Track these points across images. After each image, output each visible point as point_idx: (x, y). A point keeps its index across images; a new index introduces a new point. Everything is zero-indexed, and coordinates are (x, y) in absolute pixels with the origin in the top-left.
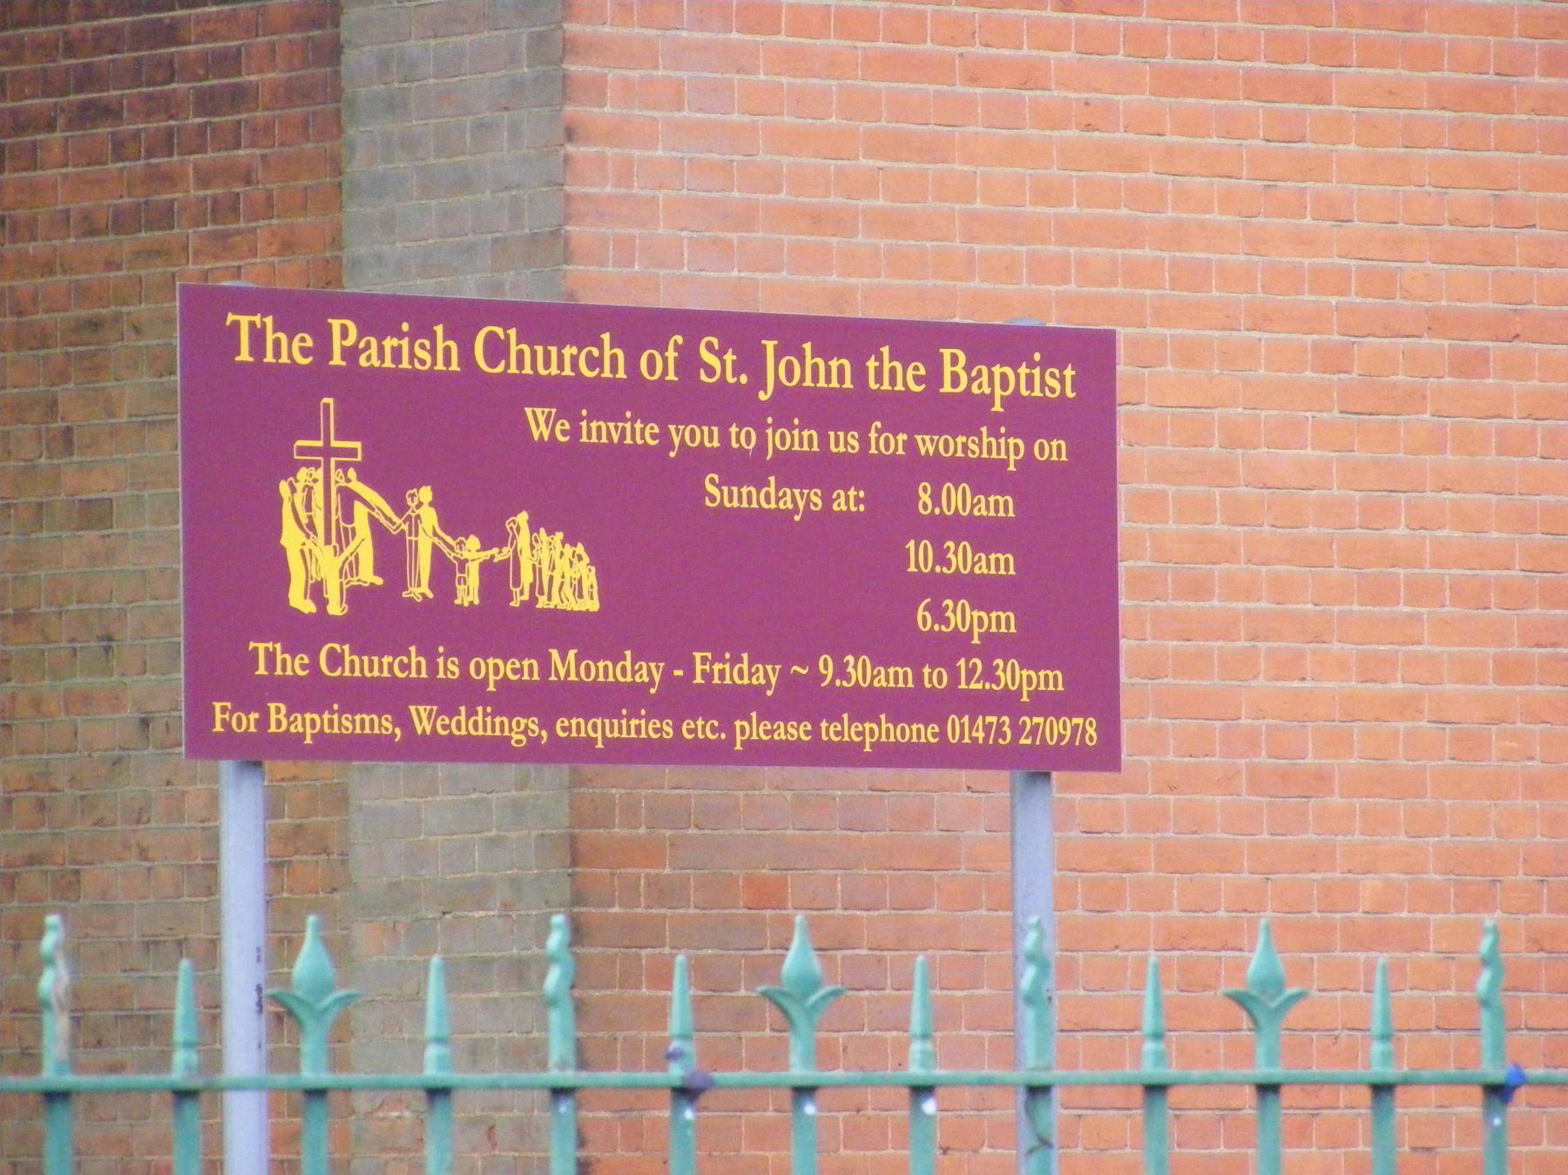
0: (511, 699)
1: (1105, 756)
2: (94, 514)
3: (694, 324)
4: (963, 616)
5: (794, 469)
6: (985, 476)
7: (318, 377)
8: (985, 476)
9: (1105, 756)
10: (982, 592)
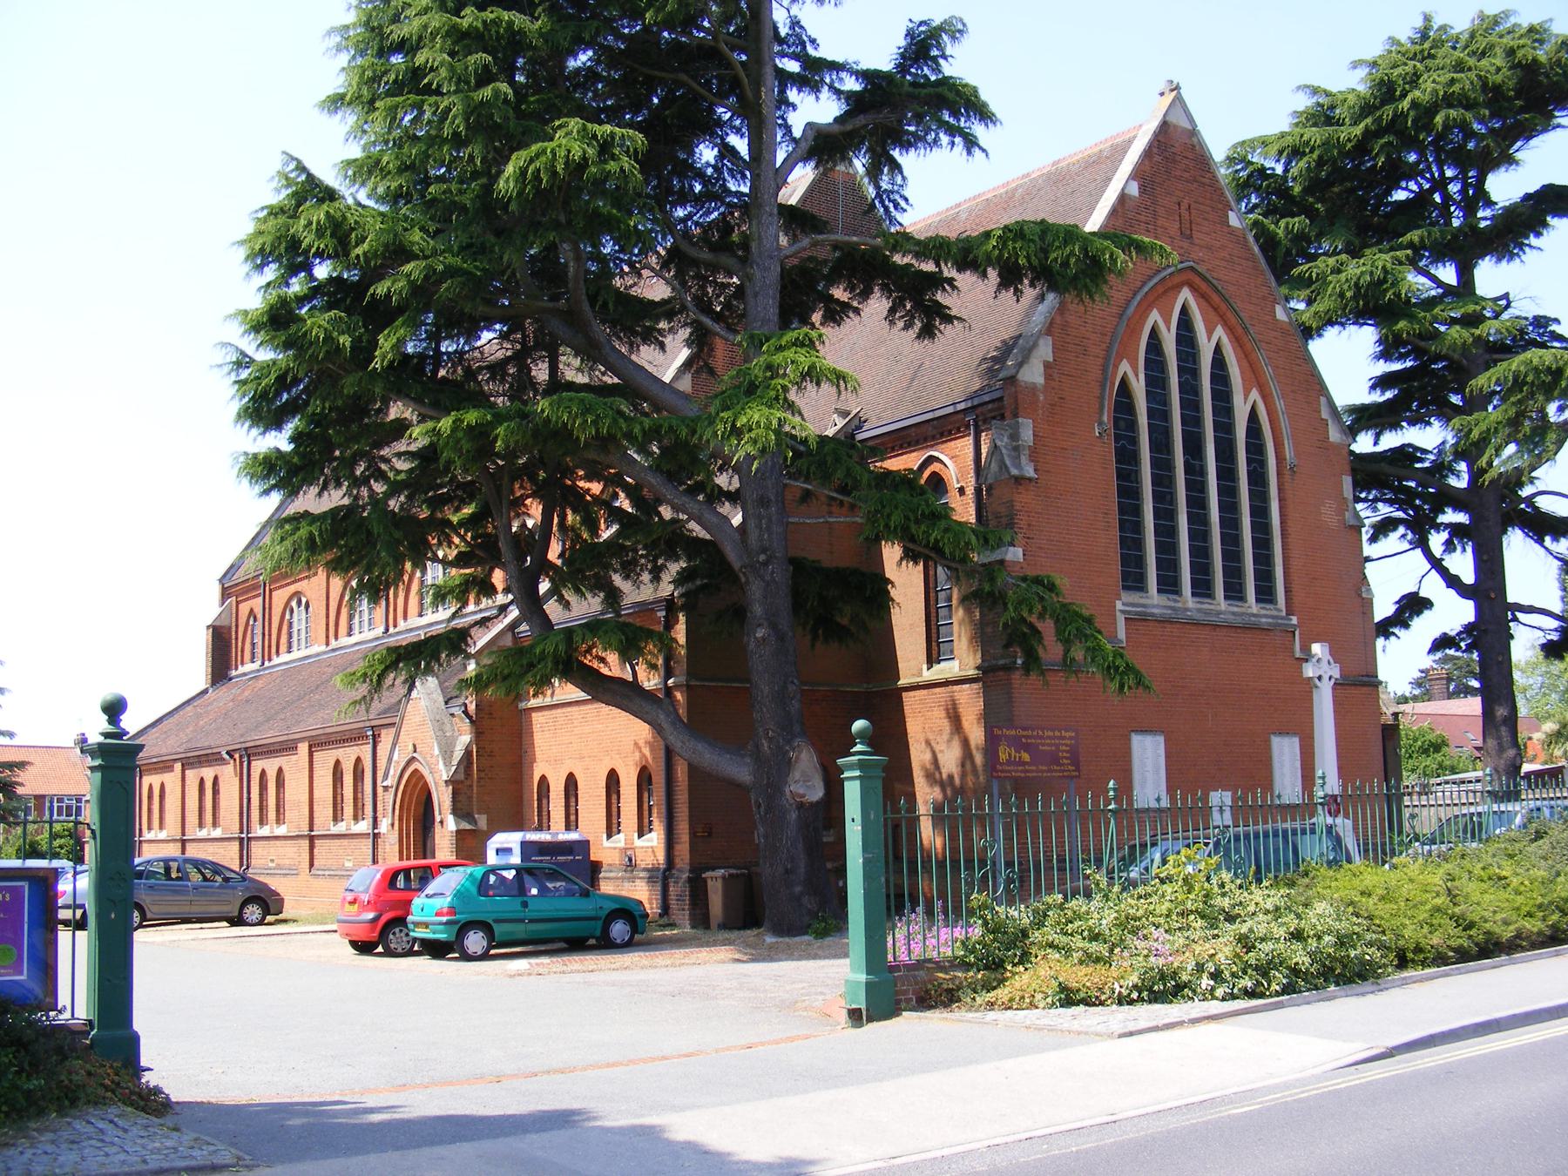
1: (1079, 777)
5: (1048, 745)
9: (1079, 777)
10: (1066, 758)
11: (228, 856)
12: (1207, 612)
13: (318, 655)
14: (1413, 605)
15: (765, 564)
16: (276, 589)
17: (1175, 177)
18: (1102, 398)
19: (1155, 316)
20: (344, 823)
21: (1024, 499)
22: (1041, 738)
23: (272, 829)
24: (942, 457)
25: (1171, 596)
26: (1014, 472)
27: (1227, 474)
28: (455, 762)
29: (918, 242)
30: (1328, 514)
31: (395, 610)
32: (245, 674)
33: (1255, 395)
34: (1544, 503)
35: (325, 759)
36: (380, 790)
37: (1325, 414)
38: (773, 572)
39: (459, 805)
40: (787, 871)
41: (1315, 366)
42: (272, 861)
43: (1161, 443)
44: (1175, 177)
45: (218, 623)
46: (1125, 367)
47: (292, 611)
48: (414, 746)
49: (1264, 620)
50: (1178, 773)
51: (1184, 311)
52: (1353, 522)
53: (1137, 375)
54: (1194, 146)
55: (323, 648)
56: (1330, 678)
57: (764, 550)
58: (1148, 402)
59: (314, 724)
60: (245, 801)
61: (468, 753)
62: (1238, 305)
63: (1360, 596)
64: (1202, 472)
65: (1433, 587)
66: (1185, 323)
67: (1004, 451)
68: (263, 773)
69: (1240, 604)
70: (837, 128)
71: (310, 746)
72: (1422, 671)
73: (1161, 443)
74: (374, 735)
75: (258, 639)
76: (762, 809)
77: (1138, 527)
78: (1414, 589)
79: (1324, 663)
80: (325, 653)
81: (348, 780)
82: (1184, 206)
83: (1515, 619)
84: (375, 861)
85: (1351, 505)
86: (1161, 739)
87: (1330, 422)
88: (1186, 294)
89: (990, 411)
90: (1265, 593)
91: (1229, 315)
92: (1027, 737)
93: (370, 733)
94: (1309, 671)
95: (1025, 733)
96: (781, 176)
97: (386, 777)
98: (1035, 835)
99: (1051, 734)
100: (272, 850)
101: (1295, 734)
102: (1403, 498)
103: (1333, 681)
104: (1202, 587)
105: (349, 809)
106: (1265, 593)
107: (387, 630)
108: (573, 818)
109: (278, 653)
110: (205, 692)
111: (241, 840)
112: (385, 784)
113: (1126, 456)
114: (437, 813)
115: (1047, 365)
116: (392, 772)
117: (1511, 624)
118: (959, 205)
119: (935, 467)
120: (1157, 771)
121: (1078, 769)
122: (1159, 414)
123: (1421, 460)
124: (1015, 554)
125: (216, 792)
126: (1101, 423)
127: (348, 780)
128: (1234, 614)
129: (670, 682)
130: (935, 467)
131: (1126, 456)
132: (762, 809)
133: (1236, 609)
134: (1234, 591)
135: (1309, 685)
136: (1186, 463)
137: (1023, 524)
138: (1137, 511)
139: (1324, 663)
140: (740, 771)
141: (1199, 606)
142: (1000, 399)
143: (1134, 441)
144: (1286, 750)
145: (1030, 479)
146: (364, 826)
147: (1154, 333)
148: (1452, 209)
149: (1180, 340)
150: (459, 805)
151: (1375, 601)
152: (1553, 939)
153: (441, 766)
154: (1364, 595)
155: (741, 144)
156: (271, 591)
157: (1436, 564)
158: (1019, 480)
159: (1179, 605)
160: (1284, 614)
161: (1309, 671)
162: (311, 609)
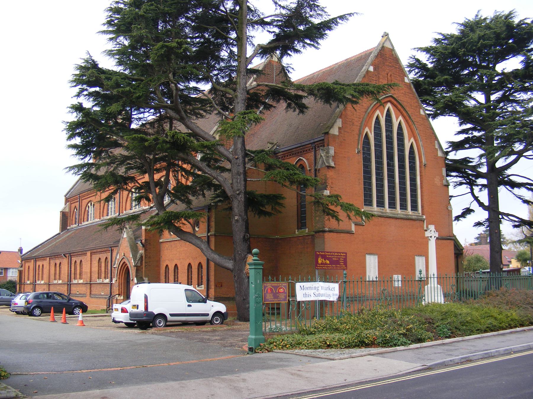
0: (326, 267)
1: (347, 269)
2: (301, 259)
3: (332, 252)
4: (342, 264)
5: (336, 258)
6: (342, 258)
7: (319, 254)
8: (342, 258)
9: (347, 269)
10: (342, 263)
11: (64, 290)
13: (97, 222)
14: (468, 211)
15: (239, 194)
16: (83, 199)
17: (386, 65)
18: (359, 140)
19: (378, 112)
21: (330, 174)
22: (333, 255)
23: (78, 281)
24: (304, 159)
26: (327, 164)
27: (402, 167)
28: (137, 260)
29: (295, 85)
31: (122, 208)
32: (72, 228)
33: (412, 140)
34: (512, 178)
35: (96, 257)
36: (113, 269)
37: (437, 147)
38: (241, 198)
39: (138, 274)
40: (244, 299)
42: (78, 292)
43: (379, 156)
44: (386, 65)
45: (63, 211)
46: (367, 130)
48: (124, 254)
49: (413, 217)
51: (388, 110)
52: (446, 184)
53: (371, 132)
54: (393, 55)
56: (435, 237)
57: (238, 190)
58: (375, 141)
59: (92, 245)
60: (69, 271)
61: (142, 257)
62: (407, 109)
63: (448, 209)
64: (393, 166)
65: (475, 206)
66: (388, 115)
67: (324, 157)
68: (76, 262)
69: (405, 211)
70: (268, 46)
71: (91, 253)
72: (479, 235)
73: (379, 156)
74: (112, 250)
75: (77, 217)
76: (236, 278)
77: (370, 184)
78: (468, 207)
79: (432, 232)
81: (103, 265)
82: (389, 75)
83: (503, 218)
85: (445, 178)
86: (376, 257)
87: (438, 149)
88: (389, 105)
89: (320, 144)
90: (414, 207)
91: (404, 112)
92: (328, 255)
93: (110, 249)
94: (427, 234)
96: (249, 60)
97: (114, 264)
98: (496, 281)
100: (78, 288)
101: (424, 256)
102: (465, 176)
103: (436, 238)
104: (392, 205)
105: (103, 275)
106: (414, 207)
107: (119, 214)
109: (84, 221)
113: (367, 160)
114: (131, 277)
115: (340, 128)
116: (117, 263)
117: (502, 220)
118: (314, 73)
119: (301, 163)
121: (346, 266)
122: (378, 146)
123: (471, 162)
124: (327, 193)
125: (42, 269)
126: (358, 149)
127: (103, 265)
128: (403, 214)
129: (209, 234)
130: (301, 163)
131: (367, 160)
132: (236, 278)
133: (404, 213)
134: (403, 207)
135: (427, 239)
137: (330, 182)
138: (370, 178)
139: (432, 232)
140: (230, 264)
142: (323, 140)
143: (370, 155)
144: (420, 261)
145: (333, 167)
146: (107, 281)
147: (377, 118)
148: (484, 77)
149: (386, 120)
151: (453, 211)
154: (449, 209)
155: (235, 49)
156: (82, 200)
157: (476, 198)
158: (329, 167)
159: (384, 211)
160: (421, 215)
161: (427, 234)
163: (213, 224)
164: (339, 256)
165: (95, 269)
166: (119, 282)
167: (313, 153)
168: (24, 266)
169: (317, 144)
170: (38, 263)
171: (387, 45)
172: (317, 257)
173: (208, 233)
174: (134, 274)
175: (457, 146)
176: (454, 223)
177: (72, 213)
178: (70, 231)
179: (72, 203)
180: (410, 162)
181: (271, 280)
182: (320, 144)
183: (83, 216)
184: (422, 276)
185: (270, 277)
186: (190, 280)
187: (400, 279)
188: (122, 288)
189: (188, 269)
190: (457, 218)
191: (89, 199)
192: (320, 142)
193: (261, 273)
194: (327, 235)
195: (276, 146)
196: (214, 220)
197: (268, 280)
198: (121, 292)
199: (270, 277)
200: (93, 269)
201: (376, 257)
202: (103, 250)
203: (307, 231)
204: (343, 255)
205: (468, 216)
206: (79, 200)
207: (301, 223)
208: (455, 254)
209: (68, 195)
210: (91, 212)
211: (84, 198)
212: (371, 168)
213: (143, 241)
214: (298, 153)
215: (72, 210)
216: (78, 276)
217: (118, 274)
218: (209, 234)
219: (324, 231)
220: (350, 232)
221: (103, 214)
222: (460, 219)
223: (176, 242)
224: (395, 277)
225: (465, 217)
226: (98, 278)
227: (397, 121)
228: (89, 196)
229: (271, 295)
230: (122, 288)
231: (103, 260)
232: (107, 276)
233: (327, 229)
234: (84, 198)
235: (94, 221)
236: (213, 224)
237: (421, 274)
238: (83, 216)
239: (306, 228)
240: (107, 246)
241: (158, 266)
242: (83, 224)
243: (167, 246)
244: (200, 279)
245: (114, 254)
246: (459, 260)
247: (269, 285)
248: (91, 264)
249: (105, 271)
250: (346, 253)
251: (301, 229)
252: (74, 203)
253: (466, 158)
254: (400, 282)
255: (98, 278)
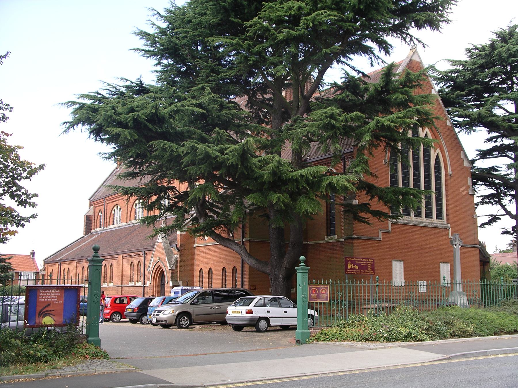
1: (374, 274)
4: (370, 269)
5: (364, 264)
6: (370, 264)
8: (370, 264)
9: (374, 274)
12: (419, 222)
13: (124, 226)
14: (494, 219)
16: (109, 203)
20: (107, 284)
23: (108, 284)
25: (407, 217)
27: (427, 177)
30: (463, 190)
32: (97, 232)
35: (127, 262)
36: (146, 272)
41: (460, 141)
47: (114, 211)
48: (159, 258)
49: (438, 225)
50: (408, 274)
55: (126, 224)
59: (123, 249)
61: (177, 261)
63: (473, 218)
64: (419, 176)
69: (431, 219)
74: (145, 254)
75: (102, 220)
76: (272, 282)
80: (126, 225)
81: (135, 268)
84: (144, 296)
86: (402, 263)
87: (464, 159)
90: (439, 216)
95: (357, 260)
97: (149, 268)
99: (365, 260)
105: (135, 278)
106: (439, 216)
108: (210, 282)
109: (109, 225)
110: (83, 237)
111: (144, 287)
112: (148, 270)
114: (166, 280)
116: (151, 266)
120: (401, 273)
121: (374, 272)
123: (499, 171)
126: (385, 160)
127: (135, 268)
128: (428, 223)
129: (244, 240)
132: (272, 282)
133: (429, 221)
134: (429, 215)
136: (414, 173)
141: (417, 220)
142: (353, 151)
144: (445, 268)
146: (140, 284)
150: (173, 278)
152: (515, 332)
153: (168, 265)
154: (474, 218)
156: (107, 204)
159: (410, 219)
160: (446, 223)
162: (121, 210)
163: (247, 230)
164: (368, 261)
165: (127, 272)
166: (153, 285)
167: (343, 163)
168: (46, 270)
169: (346, 156)
170: (63, 267)
171: (415, 58)
172: (347, 262)
173: (243, 239)
174: (170, 277)
175: (485, 154)
176: (479, 229)
177: (96, 216)
178: (94, 235)
179: (96, 207)
180: (435, 172)
181: (315, 283)
182: (349, 155)
183: (108, 219)
184: (446, 282)
185: (314, 280)
186: (224, 283)
187: (425, 284)
188: (156, 291)
189: (222, 273)
190: (483, 225)
191: (115, 203)
192: (349, 154)
193: (307, 277)
194: (355, 241)
195: (306, 157)
196: (248, 226)
197: (312, 283)
198: (156, 294)
199: (314, 280)
200: (124, 273)
201: (402, 263)
202: (136, 254)
203: (336, 238)
204: (371, 260)
205: (494, 224)
206: (104, 203)
207: (330, 230)
208: (480, 261)
209: (92, 198)
210: (118, 215)
211: (110, 202)
212: (397, 178)
213: (179, 246)
214: (328, 163)
215: (97, 214)
216: (108, 279)
217: (152, 278)
218: (244, 240)
219: (354, 239)
220: (376, 240)
221: (130, 218)
222: (486, 226)
223: (210, 247)
224: (420, 282)
225: (490, 225)
226: (130, 281)
227: (423, 132)
228: (115, 200)
229: (315, 295)
230: (156, 291)
231: (135, 264)
232: (139, 279)
233: (356, 237)
234: (110, 202)
235: (120, 225)
236: (247, 230)
237: (444, 280)
238: (108, 219)
239: (335, 235)
240: (141, 250)
241: (192, 270)
242: (109, 227)
243: (201, 250)
244: (234, 282)
245: (148, 258)
246: (486, 268)
247: (314, 286)
248: (122, 267)
249: (104, 277)
250: (374, 259)
251: (330, 236)
252: (99, 206)
253: (493, 167)
254: (419, 284)
255: (130, 281)
